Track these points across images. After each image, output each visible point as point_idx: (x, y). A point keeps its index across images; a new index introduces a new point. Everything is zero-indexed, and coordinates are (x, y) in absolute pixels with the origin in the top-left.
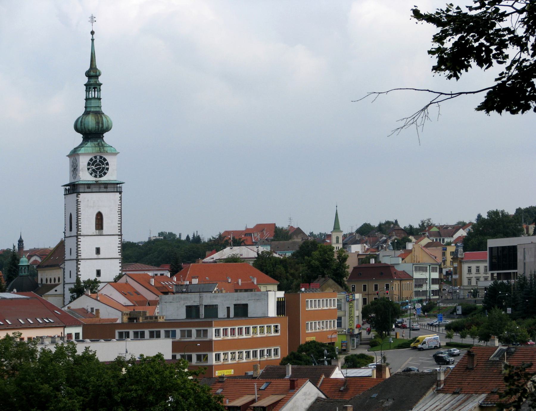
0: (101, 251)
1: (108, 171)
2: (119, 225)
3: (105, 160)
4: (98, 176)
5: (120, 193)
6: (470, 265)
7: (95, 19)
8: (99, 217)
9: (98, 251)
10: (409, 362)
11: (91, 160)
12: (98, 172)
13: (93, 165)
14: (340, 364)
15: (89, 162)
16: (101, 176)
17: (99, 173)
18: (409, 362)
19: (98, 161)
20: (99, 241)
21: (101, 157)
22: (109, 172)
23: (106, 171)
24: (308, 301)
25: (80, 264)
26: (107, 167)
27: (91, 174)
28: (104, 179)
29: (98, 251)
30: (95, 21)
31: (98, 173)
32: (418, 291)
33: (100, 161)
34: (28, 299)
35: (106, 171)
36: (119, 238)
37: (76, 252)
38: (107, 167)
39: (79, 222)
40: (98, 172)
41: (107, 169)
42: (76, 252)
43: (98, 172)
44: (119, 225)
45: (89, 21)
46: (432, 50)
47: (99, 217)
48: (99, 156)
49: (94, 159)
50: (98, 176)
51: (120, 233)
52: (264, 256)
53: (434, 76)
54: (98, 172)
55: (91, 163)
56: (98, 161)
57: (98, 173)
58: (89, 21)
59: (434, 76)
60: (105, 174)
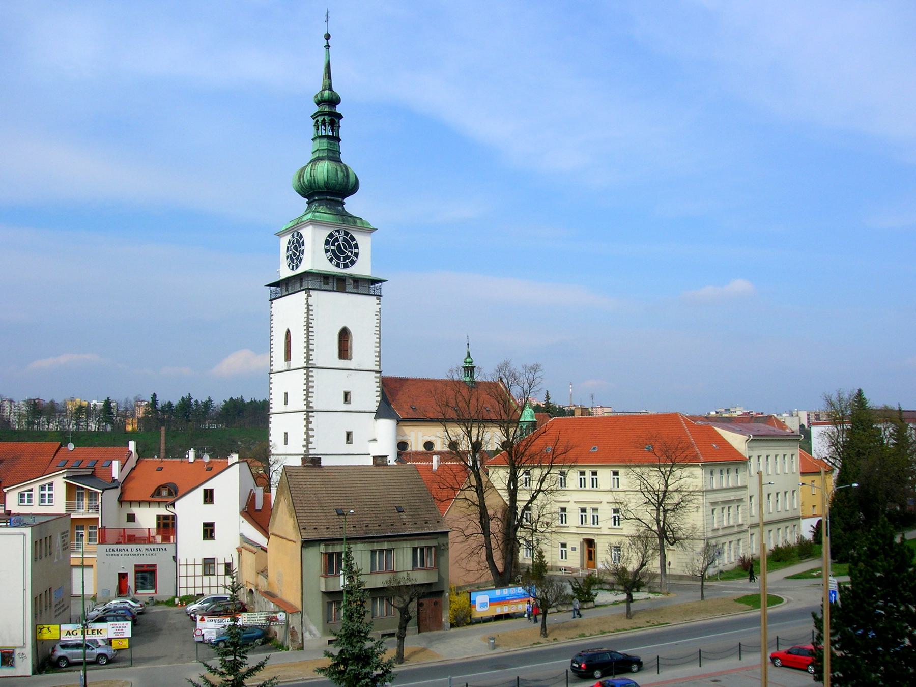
0: (353, 397)
1: (357, 258)
2: (378, 359)
3: (353, 239)
4: (342, 265)
5: (379, 296)
6: (618, 489)
8: (344, 335)
10: (775, 427)
11: (331, 235)
12: (342, 258)
13: (345, 240)
15: (328, 238)
16: (346, 266)
17: (352, 249)
18: (775, 427)
19: (333, 248)
20: (343, 381)
21: (346, 233)
22: (359, 261)
25: (304, 446)
27: (331, 260)
28: (353, 270)
31: (342, 260)
33: (333, 244)
34: (72, 659)
36: (375, 377)
37: (340, 117)
42: (340, 117)
44: (378, 359)
47: (344, 335)
50: (342, 265)
51: (377, 368)
52: (445, 522)
54: (342, 258)
56: (333, 248)
57: (342, 260)
60: (353, 262)
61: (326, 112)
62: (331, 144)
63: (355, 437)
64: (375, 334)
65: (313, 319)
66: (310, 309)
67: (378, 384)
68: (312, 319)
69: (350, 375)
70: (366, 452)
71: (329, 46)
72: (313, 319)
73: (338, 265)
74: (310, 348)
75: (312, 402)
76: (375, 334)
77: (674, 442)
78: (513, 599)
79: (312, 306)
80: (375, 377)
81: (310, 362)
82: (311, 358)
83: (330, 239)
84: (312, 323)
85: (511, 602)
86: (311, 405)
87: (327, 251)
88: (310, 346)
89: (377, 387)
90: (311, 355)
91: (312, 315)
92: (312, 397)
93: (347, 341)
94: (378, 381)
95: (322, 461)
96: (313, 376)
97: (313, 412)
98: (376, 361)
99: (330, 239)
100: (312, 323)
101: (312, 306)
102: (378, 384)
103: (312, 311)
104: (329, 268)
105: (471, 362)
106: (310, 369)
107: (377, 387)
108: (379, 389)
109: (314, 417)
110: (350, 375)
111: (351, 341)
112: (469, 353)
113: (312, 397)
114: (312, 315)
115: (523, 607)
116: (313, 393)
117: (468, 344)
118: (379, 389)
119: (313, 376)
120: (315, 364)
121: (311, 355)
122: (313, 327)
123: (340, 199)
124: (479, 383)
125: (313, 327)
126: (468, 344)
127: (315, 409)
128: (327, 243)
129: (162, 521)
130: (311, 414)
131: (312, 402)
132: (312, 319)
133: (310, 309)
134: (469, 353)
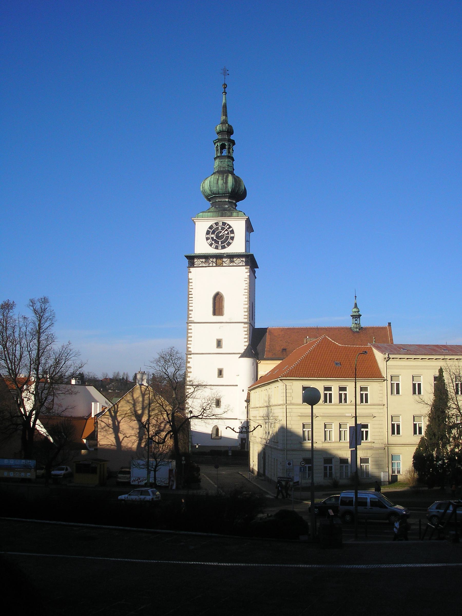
0: (224, 343)
4: (220, 248)
7: (228, 73)
9: (219, 343)
14: (174, 470)
15: (209, 230)
16: (223, 247)
23: (231, 241)
24: (327, 466)
26: (232, 235)
27: (211, 245)
29: (219, 343)
30: (228, 74)
32: (331, 466)
33: (213, 233)
35: (231, 241)
36: (244, 327)
38: (232, 235)
39: (190, 305)
40: (220, 243)
41: (232, 238)
43: (220, 243)
45: (221, 73)
46: (149, 463)
48: (221, 223)
49: (215, 226)
50: (220, 248)
53: (278, 387)
55: (211, 231)
58: (221, 73)
59: (278, 387)
60: (229, 244)
61: (227, 139)
62: (221, 162)
63: (224, 373)
64: (244, 295)
65: (193, 289)
66: (190, 281)
67: (246, 333)
68: (191, 289)
69: (222, 327)
70: (235, 384)
71: (226, 93)
72: (193, 289)
73: (217, 248)
74: (190, 309)
75: (190, 348)
76: (244, 295)
77: (11, 340)
78: (18, 468)
79: (191, 279)
80: (244, 327)
81: (190, 319)
82: (190, 316)
83: (210, 230)
84: (191, 292)
85: (16, 469)
86: (189, 349)
87: (207, 239)
88: (190, 307)
89: (245, 335)
90: (191, 314)
91: (192, 286)
92: (191, 344)
93: (222, 302)
94: (246, 330)
95: (247, 395)
96: (191, 329)
97: (191, 354)
98: (245, 315)
99: (210, 230)
100: (191, 292)
101: (191, 279)
102: (246, 333)
103: (192, 282)
104: (212, 251)
105: (358, 312)
106: (190, 324)
107: (245, 335)
108: (247, 336)
109: (191, 358)
110: (222, 327)
111: (224, 302)
112: (356, 304)
113: (191, 344)
114: (192, 286)
115: (25, 475)
116: (191, 341)
117: (356, 297)
118: (247, 336)
119: (191, 329)
120: (194, 321)
121: (191, 314)
122: (192, 294)
123: (234, 201)
124: (366, 329)
125: (192, 294)
126: (356, 297)
127: (192, 352)
128: (208, 233)
129: (352, 451)
130: (189, 356)
131: (190, 348)
132: (191, 289)
133: (190, 281)
134: (356, 304)
